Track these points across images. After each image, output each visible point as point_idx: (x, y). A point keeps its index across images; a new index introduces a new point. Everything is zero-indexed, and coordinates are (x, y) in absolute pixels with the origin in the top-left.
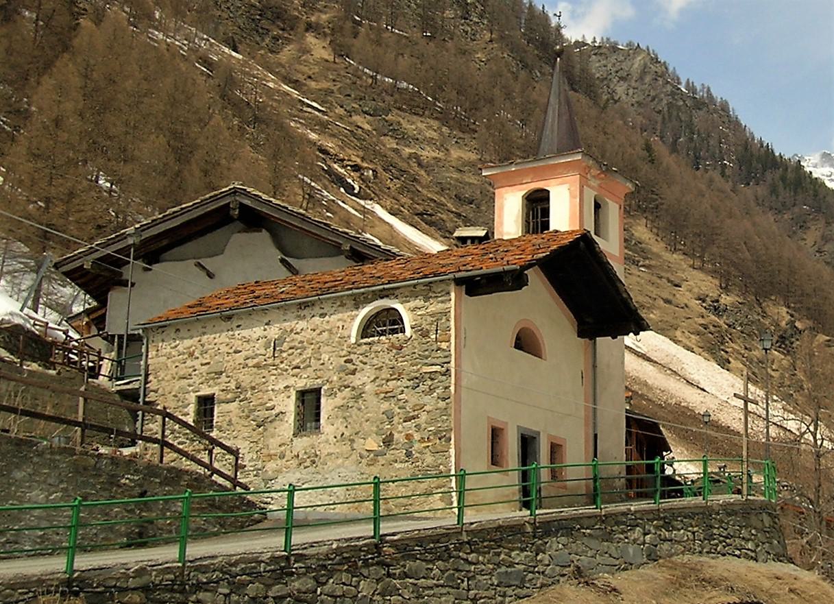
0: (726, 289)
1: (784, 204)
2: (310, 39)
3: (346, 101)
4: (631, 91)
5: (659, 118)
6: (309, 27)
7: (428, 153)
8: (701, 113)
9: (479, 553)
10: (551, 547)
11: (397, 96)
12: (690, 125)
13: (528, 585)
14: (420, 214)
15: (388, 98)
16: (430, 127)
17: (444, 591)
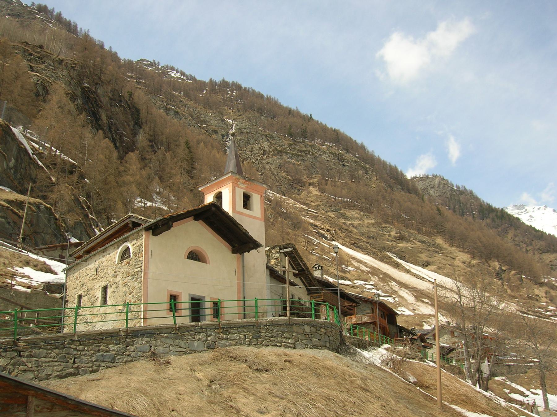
0: (473, 258)
1: (498, 225)
2: (311, 188)
3: (325, 208)
4: (436, 192)
5: (447, 200)
6: (310, 184)
7: (356, 223)
8: (463, 196)
9: (84, 345)
10: (137, 342)
11: (343, 204)
12: (459, 201)
13: (117, 361)
14: (353, 244)
15: (340, 205)
16: (356, 213)
17: (57, 364)
